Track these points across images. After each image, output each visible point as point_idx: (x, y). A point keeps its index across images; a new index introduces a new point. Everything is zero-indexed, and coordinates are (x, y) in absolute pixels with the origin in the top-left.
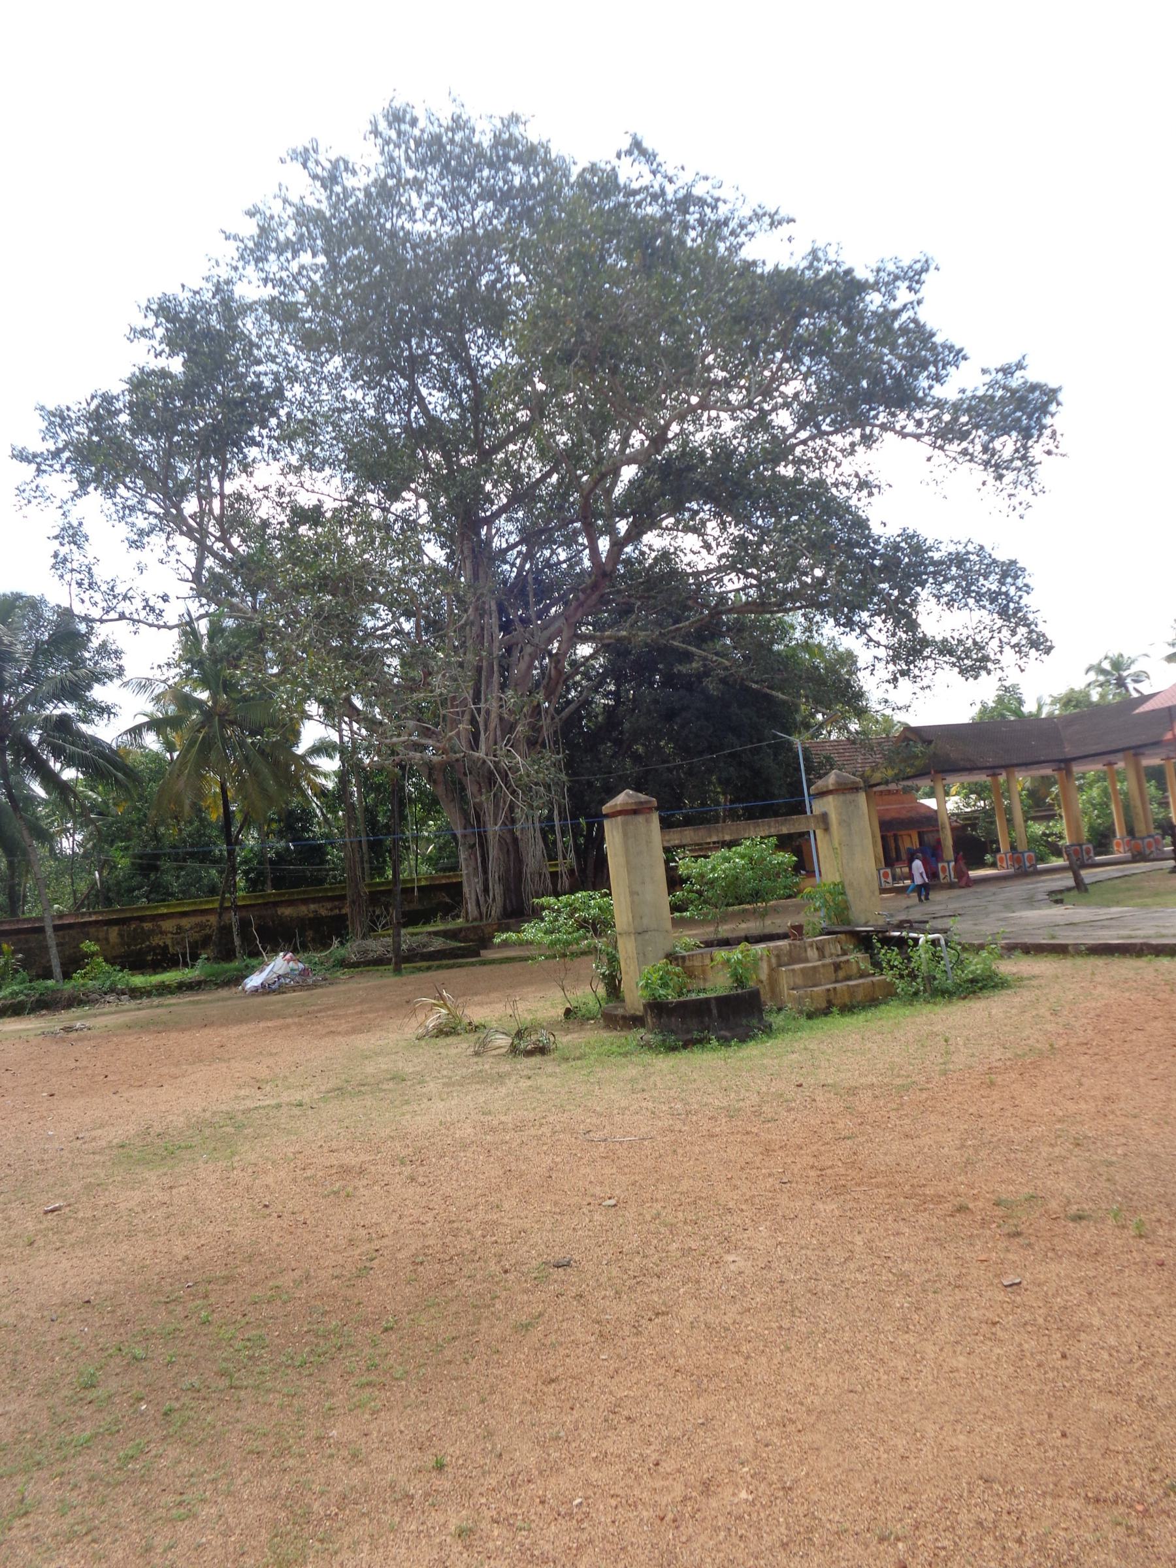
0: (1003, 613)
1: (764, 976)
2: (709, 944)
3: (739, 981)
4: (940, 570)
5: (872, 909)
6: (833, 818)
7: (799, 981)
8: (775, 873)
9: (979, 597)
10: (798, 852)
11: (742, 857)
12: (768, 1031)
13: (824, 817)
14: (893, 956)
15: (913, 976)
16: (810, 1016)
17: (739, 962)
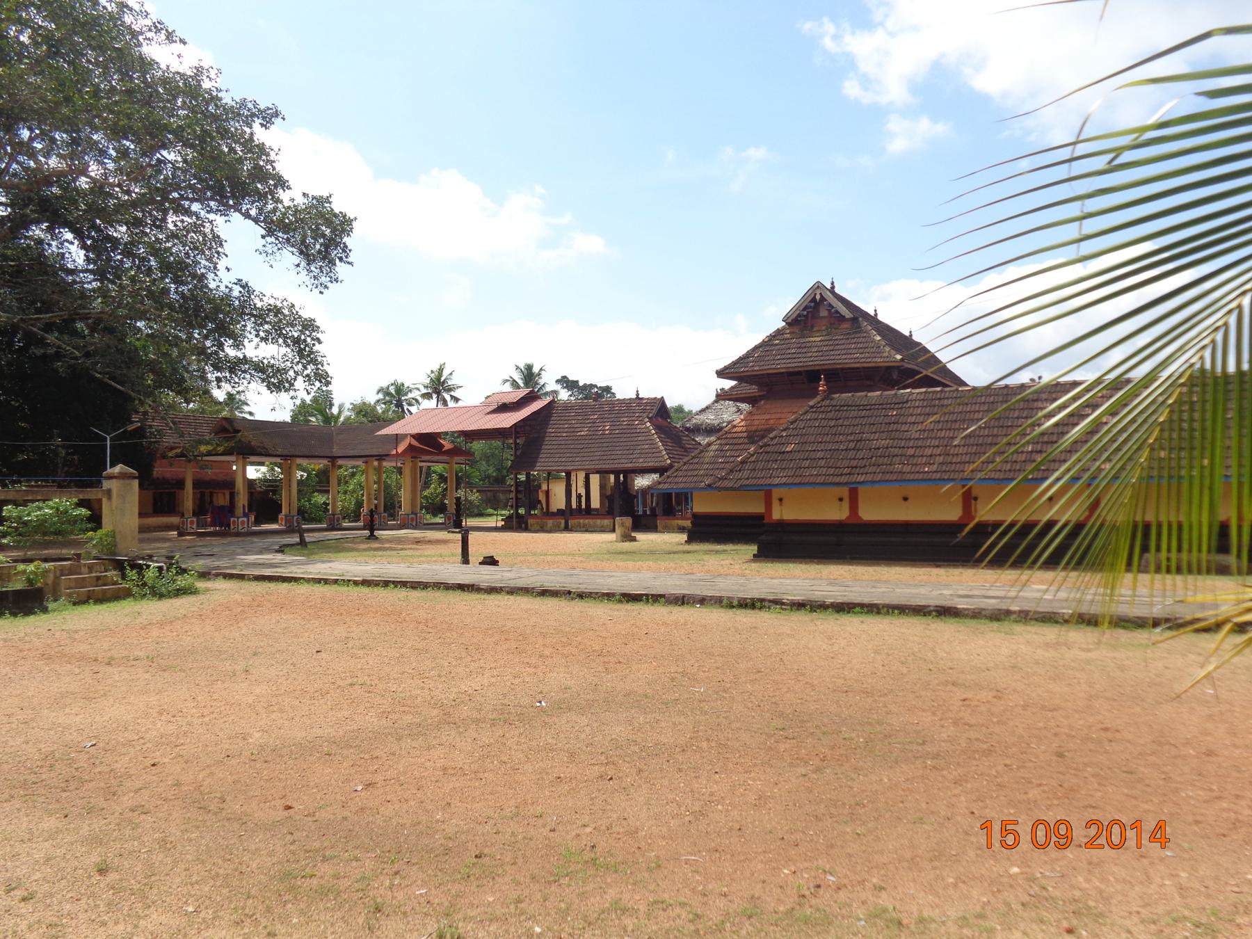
0: (300, 353)
1: (50, 581)
2: (16, 561)
3: (30, 581)
4: (260, 317)
5: (130, 547)
6: (114, 492)
7: (73, 585)
8: (75, 521)
9: (285, 337)
10: (89, 508)
11: (52, 508)
12: (45, 610)
13: (109, 492)
14: (132, 574)
15: (145, 584)
16: (74, 604)
17: (32, 572)
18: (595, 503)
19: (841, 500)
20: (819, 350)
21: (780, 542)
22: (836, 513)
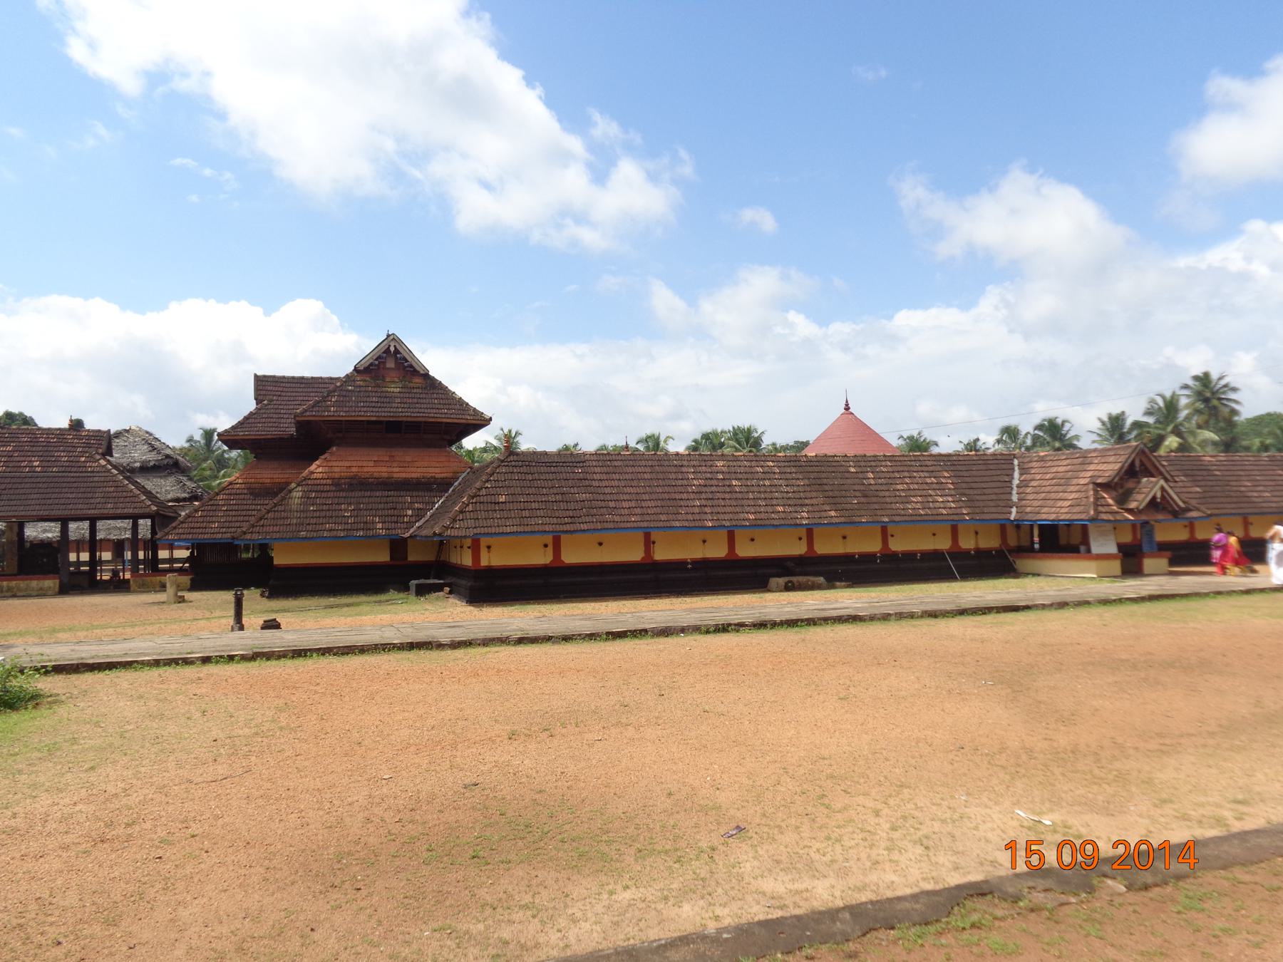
18: (1037, 546)
19: (546, 546)
20: (396, 403)
21: (492, 587)
22: (542, 558)
